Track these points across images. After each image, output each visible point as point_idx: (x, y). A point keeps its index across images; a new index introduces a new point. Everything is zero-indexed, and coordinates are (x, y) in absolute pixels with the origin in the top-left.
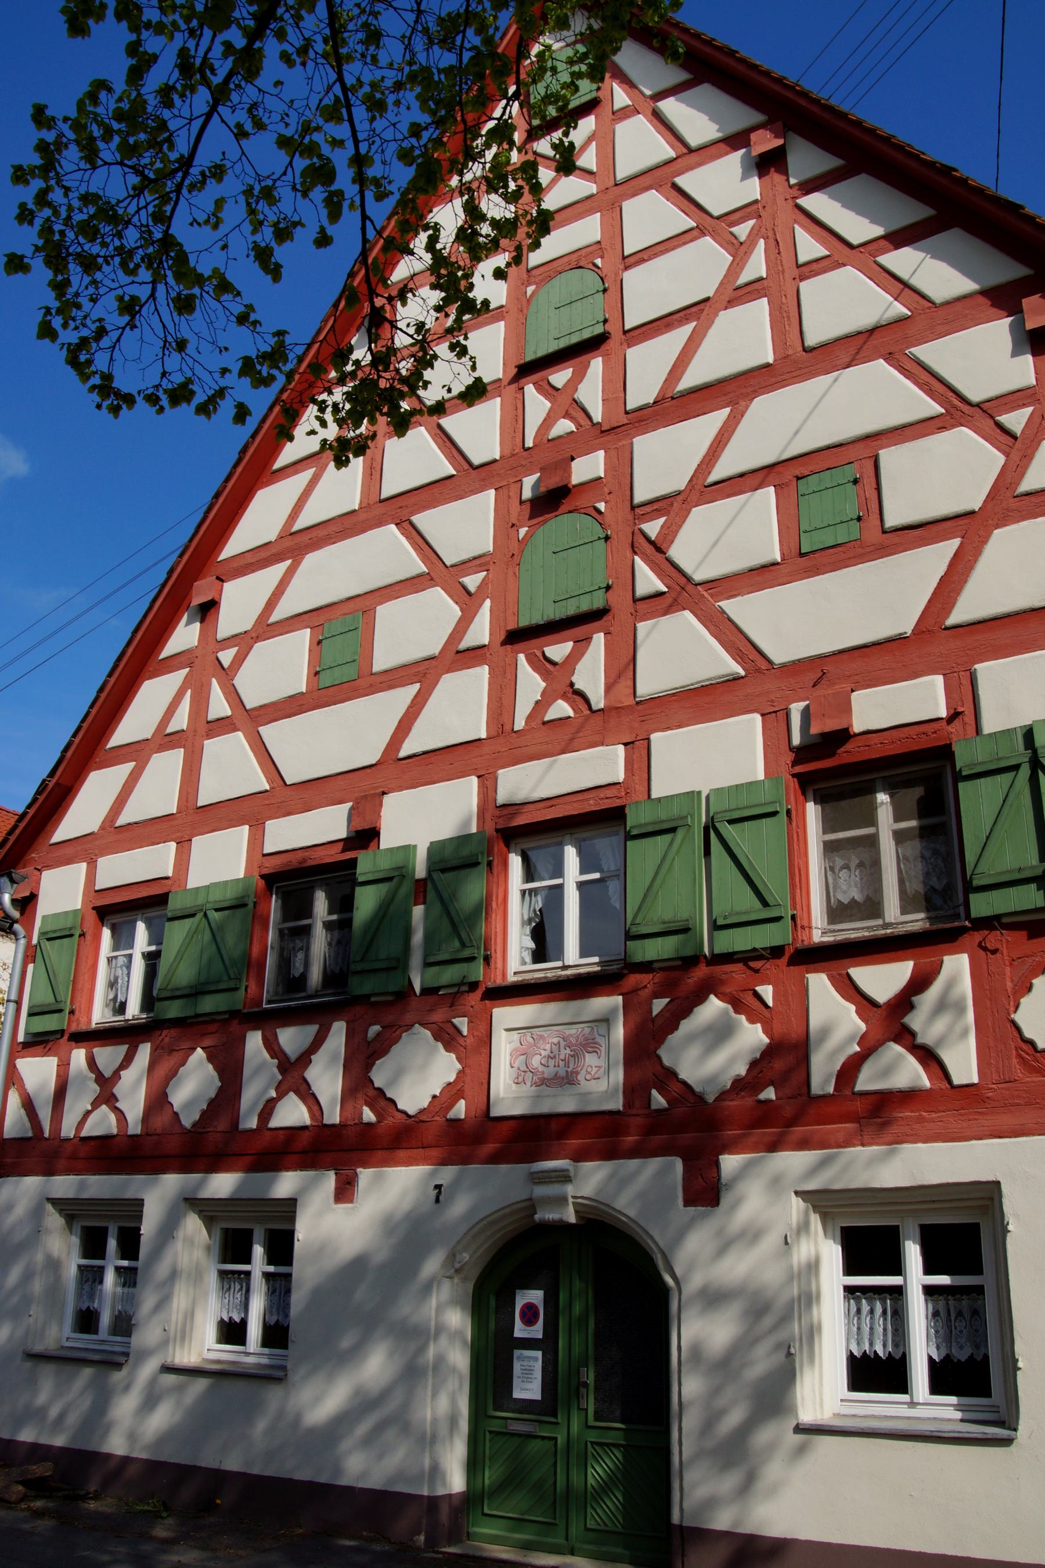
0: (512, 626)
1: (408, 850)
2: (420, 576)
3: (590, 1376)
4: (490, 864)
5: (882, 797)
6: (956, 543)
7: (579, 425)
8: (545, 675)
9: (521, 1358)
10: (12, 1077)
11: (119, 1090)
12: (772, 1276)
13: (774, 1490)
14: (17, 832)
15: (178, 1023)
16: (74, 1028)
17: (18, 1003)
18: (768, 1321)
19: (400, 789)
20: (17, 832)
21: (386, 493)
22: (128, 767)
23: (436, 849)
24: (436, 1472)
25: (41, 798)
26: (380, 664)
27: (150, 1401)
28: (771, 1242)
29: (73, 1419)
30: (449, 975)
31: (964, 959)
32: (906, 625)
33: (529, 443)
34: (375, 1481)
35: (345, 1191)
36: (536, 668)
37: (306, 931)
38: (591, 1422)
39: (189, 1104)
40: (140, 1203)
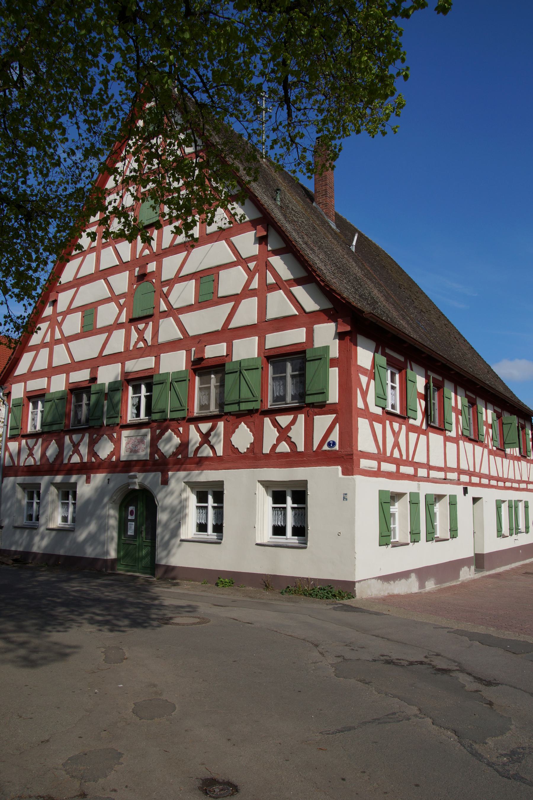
0: (131, 317)
1: (104, 384)
2: (109, 298)
3: (144, 528)
4: (122, 390)
5: (213, 376)
6: (233, 303)
7: (150, 252)
8: (138, 334)
9: (130, 524)
10: (7, 448)
11: (34, 452)
12: (176, 502)
13: (174, 554)
14: (4, 372)
15: (48, 433)
16: (22, 434)
17: (7, 426)
18: (175, 514)
19: (103, 365)
20: (4, 372)
21: (101, 269)
22: (34, 353)
23: (110, 383)
24: (107, 553)
25: (10, 362)
26: (99, 325)
27: (42, 538)
28: (176, 494)
29: (24, 543)
30: (111, 421)
31: (222, 423)
32: (219, 328)
33: (138, 257)
34: (92, 556)
35: (88, 481)
36: (136, 331)
37: (81, 406)
38: (144, 540)
39: (51, 456)
40: (40, 484)
